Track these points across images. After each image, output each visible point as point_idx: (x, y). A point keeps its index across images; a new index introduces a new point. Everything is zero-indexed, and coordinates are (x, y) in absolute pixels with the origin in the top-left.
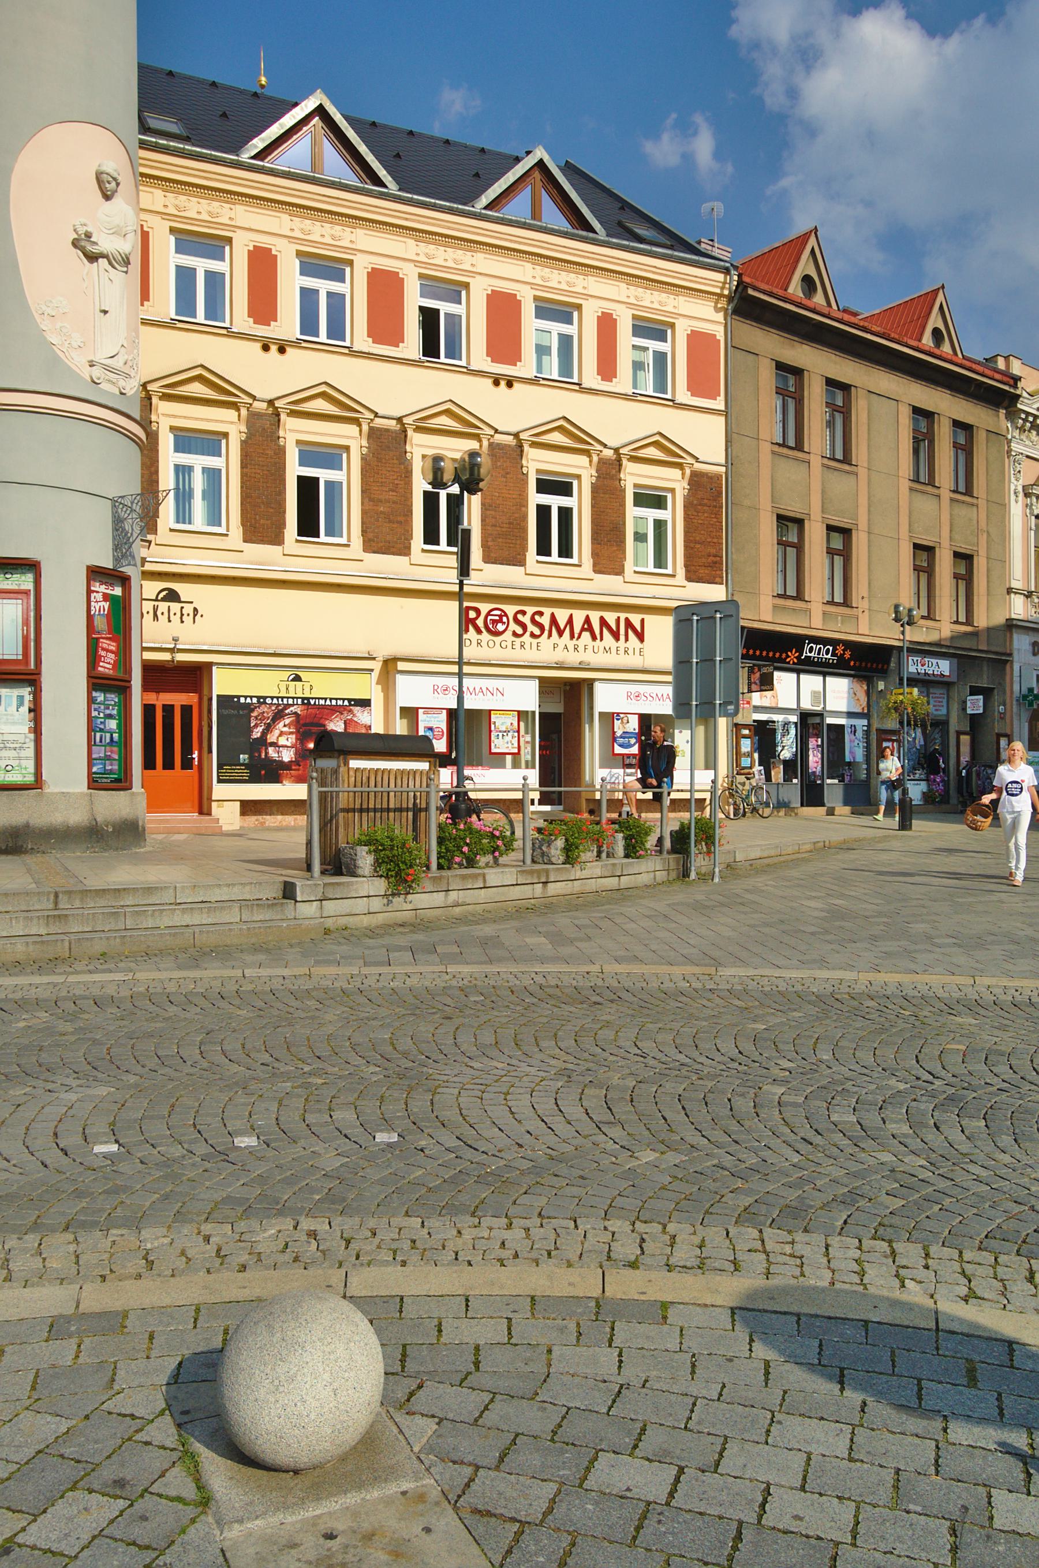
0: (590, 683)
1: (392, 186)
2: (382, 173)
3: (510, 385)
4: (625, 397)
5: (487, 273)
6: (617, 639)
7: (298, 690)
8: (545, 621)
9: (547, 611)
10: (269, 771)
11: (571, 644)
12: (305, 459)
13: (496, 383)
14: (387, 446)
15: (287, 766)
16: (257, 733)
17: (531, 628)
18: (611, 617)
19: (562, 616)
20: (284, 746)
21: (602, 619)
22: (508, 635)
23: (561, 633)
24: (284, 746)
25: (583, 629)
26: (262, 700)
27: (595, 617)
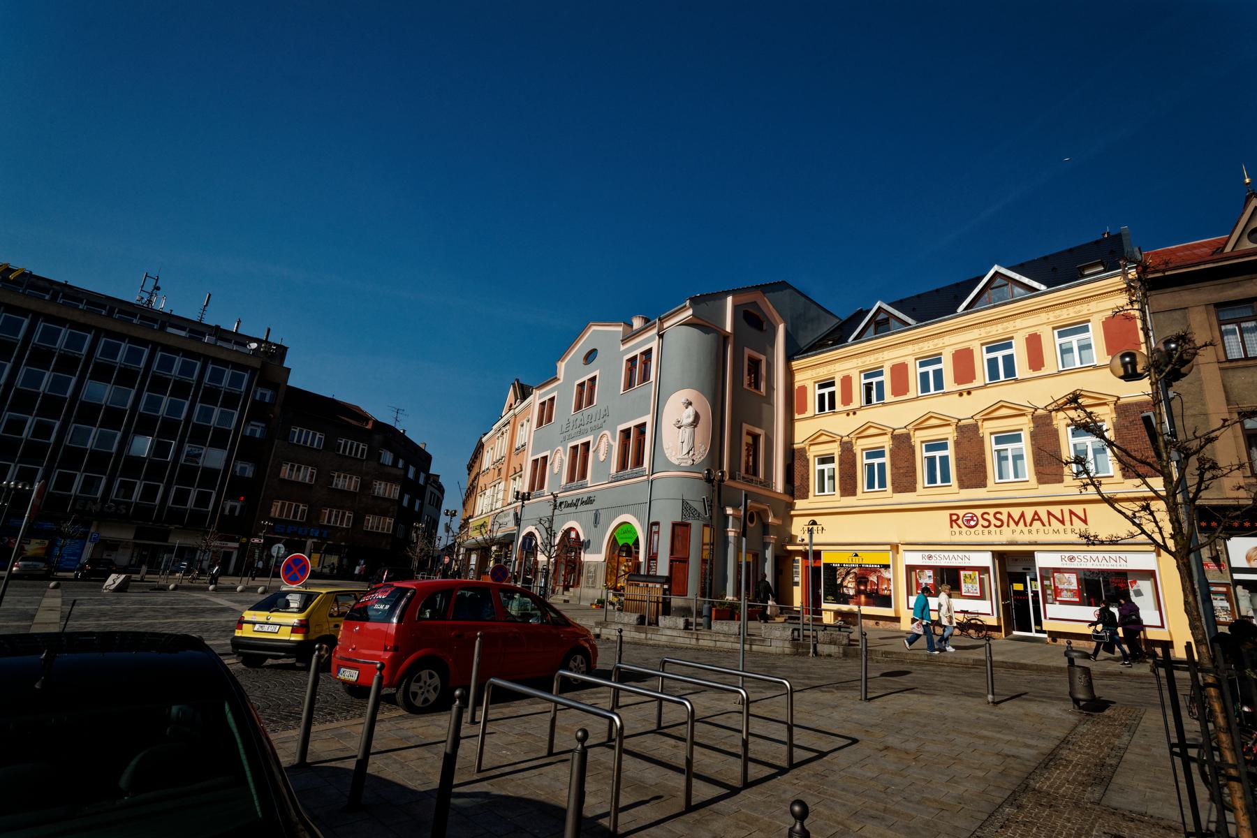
0: (1031, 554)
1: (1043, 288)
2: (1035, 284)
3: (969, 393)
4: (1059, 373)
5: (1019, 330)
6: (1063, 522)
7: (857, 561)
8: (1004, 517)
9: (1005, 511)
10: (845, 599)
11: (1026, 530)
12: (999, 441)
13: (961, 395)
14: (902, 443)
15: (851, 597)
16: (839, 581)
17: (993, 521)
18: (1056, 510)
19: (1016, 512)
20: (850, 587)
21: (1049, 513)
22: (979, 527)
23: (1017, 524)
24: (850, 587)
25: (1033, 519)
26: (841, 565)
27: (1042, 511)
